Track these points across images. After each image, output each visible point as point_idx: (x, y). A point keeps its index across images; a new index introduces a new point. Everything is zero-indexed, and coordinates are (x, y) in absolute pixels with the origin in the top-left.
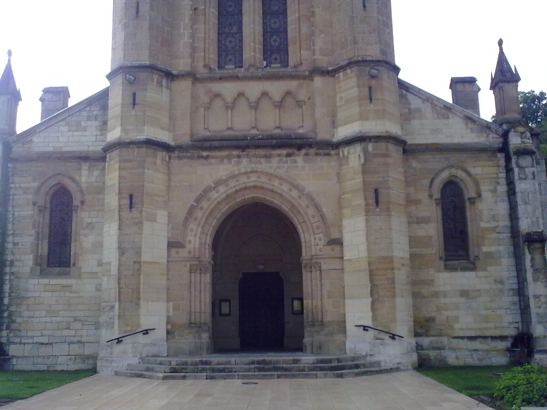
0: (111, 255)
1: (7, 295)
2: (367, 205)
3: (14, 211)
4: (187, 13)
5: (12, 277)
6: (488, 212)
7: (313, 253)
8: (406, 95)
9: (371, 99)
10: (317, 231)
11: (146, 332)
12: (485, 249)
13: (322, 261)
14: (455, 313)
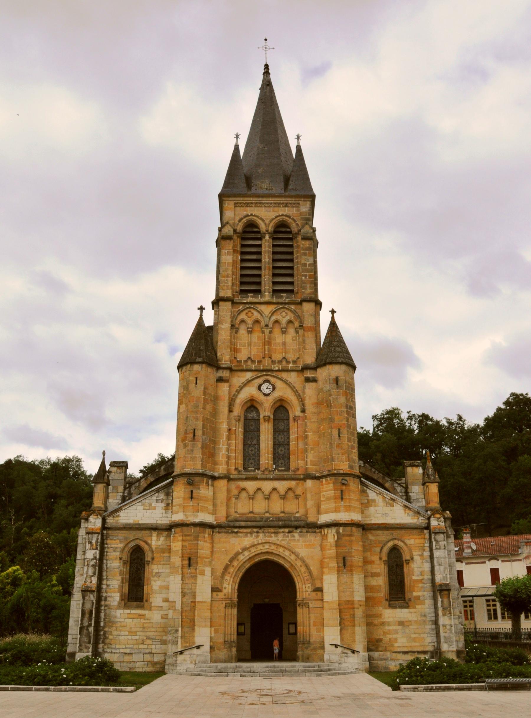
0: (175, 596)
1: (102, 620)
2: (338, 567)
3: (107, 563)
4: (225, 434)
5: (106, 608)
6: (417, 569)
7: (304, 597)
8: (366, 490)
9: (342, 498)
10: (306, 582)
11: (198, 647)
12: (415, 594)
13: (310, 602)
14: (394, 636)
